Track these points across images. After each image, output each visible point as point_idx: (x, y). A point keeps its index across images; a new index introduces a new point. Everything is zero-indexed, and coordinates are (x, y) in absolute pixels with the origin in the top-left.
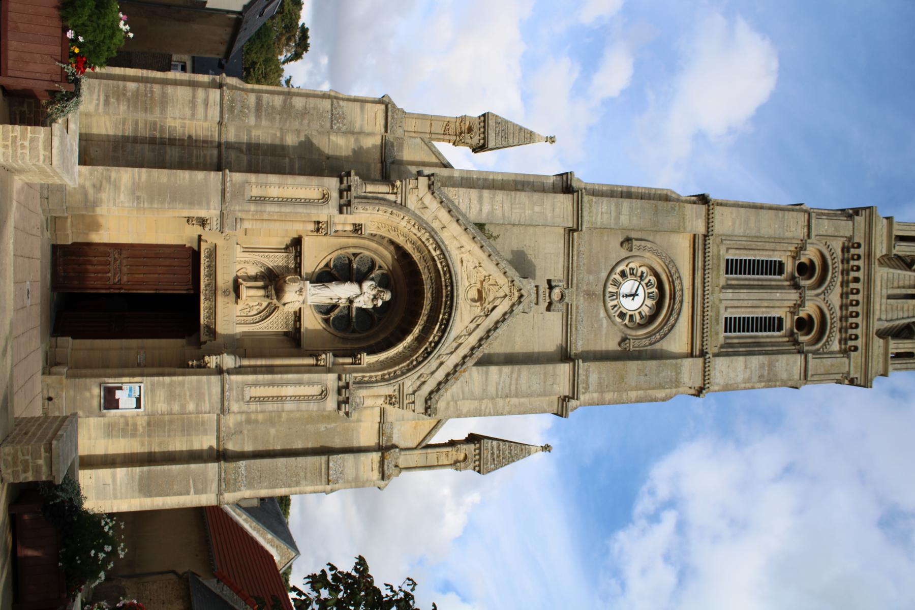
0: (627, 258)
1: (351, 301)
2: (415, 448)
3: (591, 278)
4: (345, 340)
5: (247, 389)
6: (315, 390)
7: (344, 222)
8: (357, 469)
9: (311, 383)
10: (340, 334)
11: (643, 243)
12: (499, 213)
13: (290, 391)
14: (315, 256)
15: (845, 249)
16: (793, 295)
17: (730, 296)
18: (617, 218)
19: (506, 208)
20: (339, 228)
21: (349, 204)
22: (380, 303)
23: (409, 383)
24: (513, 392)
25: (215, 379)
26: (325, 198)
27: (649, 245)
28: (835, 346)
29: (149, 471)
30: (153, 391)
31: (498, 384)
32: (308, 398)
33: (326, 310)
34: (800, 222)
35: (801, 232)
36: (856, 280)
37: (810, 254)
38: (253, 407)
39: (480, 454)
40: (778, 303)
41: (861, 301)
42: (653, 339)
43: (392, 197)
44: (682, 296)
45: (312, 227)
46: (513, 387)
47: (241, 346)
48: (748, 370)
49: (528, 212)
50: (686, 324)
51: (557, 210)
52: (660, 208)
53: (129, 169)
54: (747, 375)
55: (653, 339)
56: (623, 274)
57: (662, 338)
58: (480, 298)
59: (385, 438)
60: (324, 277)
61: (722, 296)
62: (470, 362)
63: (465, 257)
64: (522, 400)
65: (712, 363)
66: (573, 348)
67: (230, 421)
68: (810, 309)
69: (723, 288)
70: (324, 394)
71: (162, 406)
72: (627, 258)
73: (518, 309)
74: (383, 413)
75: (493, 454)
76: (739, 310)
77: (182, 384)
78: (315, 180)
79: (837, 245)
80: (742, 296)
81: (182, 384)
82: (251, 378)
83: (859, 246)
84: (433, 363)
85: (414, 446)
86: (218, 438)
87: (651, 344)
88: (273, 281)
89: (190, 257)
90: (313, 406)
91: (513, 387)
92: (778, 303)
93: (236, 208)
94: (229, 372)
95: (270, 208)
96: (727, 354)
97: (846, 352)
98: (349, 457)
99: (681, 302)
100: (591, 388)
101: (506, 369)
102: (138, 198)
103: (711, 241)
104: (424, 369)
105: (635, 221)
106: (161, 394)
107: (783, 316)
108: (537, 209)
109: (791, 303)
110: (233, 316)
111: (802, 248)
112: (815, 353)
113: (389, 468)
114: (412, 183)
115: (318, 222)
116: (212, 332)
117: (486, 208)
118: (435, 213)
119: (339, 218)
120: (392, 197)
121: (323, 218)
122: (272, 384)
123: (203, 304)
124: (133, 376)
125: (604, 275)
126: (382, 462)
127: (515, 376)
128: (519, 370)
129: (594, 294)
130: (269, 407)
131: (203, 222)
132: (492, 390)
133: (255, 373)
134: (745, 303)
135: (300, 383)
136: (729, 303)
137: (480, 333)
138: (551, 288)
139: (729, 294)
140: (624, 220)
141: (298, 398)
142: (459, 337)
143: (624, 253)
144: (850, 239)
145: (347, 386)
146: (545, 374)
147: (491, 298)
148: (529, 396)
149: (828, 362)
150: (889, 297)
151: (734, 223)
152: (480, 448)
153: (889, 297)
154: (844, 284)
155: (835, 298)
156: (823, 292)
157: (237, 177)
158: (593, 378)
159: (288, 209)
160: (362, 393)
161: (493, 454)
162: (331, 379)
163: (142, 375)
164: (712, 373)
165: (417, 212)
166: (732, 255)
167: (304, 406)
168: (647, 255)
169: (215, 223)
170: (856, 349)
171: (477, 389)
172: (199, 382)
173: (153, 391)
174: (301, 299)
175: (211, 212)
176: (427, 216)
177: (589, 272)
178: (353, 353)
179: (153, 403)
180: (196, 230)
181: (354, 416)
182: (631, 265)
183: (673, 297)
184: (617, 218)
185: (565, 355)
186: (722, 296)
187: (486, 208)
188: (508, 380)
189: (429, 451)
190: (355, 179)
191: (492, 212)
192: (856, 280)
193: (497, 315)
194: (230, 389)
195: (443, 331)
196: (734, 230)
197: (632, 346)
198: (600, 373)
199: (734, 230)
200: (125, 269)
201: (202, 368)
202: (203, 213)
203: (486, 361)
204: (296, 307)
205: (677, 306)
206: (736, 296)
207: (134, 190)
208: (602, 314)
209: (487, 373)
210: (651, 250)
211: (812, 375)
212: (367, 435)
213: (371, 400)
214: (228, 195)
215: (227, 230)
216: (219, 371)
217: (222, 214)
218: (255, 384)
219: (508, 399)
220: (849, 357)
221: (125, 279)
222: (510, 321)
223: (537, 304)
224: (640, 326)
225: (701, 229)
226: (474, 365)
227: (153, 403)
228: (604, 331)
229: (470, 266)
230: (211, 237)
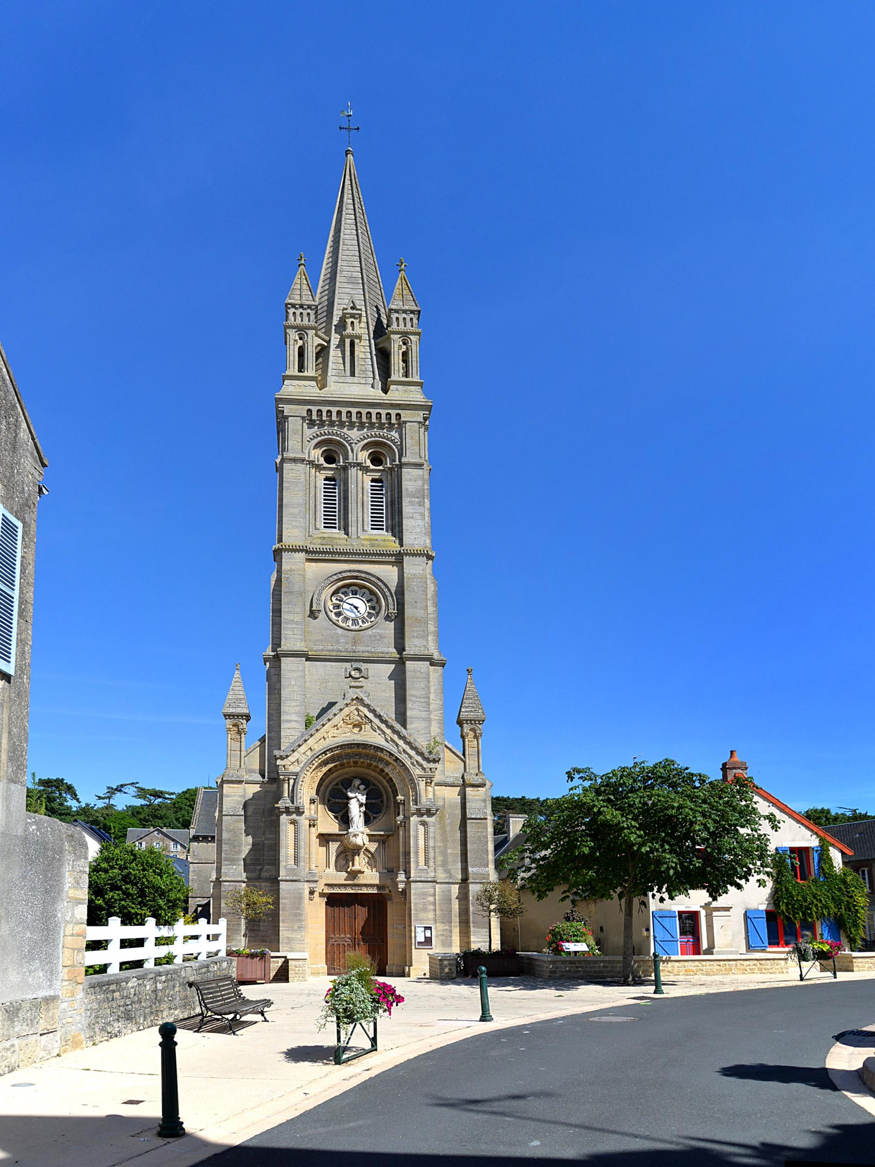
0: (326, 613)
1: (361, 805)
2: (465, 762)
3: (342, 640)
4: (388, 807)
5: (420, 867)
6: (421, 829)
7: (309, 810)
8: (477, 800)
9: (417, 831)
10: (384, 810)
11: (314, 601)
12: (297, 709)
13: (421, 843)
14: (329, 824)
15: (312, 424)
16: (353, 472)
17: (354, 529)
18: (297, 623)
19: (294, 704)
20: (313, 812)
21: (297, 808)
22: (362, 787)
23: (417, 772)
24: (426, 700)
25: (413, 885)
26: (294, 822)
27: (316, 596)
28: (395, 434)
29: (473, 923)
30: (420, 920)
31: (420, 710)
32: (426, 833)
33: (367, 822)
34: (292, 467)
35: (300, 467)
36: (339, 413)
37: (317, 455)
38: (431, 864)
39: (471, 721)
40: (361, 484)
41: (358, 410)
42: (388, 594)
43: (292, 782)
44: (354, 571)
45: (312, 829)
46: (423, 700)
47: (390, 872)
48: (415, 515)
49: (296, 688)
50: (369, 1060)
51: (293, 668)
52: (287, 590)
53: (281, 933)
54: (419, 517)
55: (388, 594)
56: (338, 614)
57: (387, 587)
58: (358, 725)
59: (456, 782)
60: (345, 820)
61: (354, 537)
62: (403, 732)
63: (331, 734)
64: (432, 691)
65: (409, 548)
66: (393, 655)
67: (441, 876)
68: (363, 457)
69: (347, 534)
70: (424, 824)
71: (431, 915)
72: (326, 613)
73: (367, 701)
74: (437, 785)
75: (471, 711)
76: (365, 519)
77: (416, 904)
78: (282, 828)
79: (309, 432)
80: (354, 518)
81: (416, 904)
82: (412, 865)
83: (309, 411)
84: (403, 757)
85: (463, 764)
86: (453, 883)
87: (392, 596)
88: (347, 853)
89: (333, 901)
90: (431, 829)
91: (423, 700)
92: (361, 484)
93: (304, 873)
94: (408, 877)
95: (302, 853)
96: (401, 532)
97: (401, 425)
98: (468, 805)
99: (359, 571)
100: (425, 643)
101: (409, 705)
102: (299, 927)
103: (311, 547)
104: (408, 763)
105: (298, 610)
106: (422, 915)
107: (370, 478)
108: (293, 683)
109: (360, 473)
110: (370, 877)
111: (311, 463)
112: (401, 456)
113: (478, 780)
114: (281, 770)
115: (310, 825)
116: (378, 887)
117: (294, 717)
118: (302, 755)
119: (307, 813)
120: (292, 782)
121: (307, 822)
122: (417, 853)
123: (365, 891)
124: (411, 931)
125: (340, 631)
126: (473, 786)
127: (414, 699)
128: (410, 696)
129: (354, 638)
130: (431, 855)
131: (312, 893)
132: (424, 715)
133: (409, 863)
134: (360, 515)
135: (416, 837)
136: (360, 530)
137: (383, 727)
138: (350, 676)
139: (352, 530)
140: (297, 618)
141: (426, 839)
142: (386, 740)
143: (322, 615)
144: (303, 418)
145: (419, 810)
146: (413, 678)
147: (359, 718)
148: (429, 687)
149: (409, 442)
150: (353, 374)
151: (297, 527)
152: (467, 721)
153: (353, 374)
154: (342, 424)
155: (354, 434)
156: (350, 444)
157: (282, 872)
158: (417, 642)
159: (302, 844)
160: (424, 799)
161: (471, 711)
162: (414, 819)
163: (410, 926)
164: (416, 548)
165: (301, 765)
166: (321, 524)
167: (431, 835)
168: (323, 597)
169: (313, 885)
170: (398, 415)
171: (423, 724)
172: (414, 894)
173: (420, 920)
174: (360, 835)
175: (306, 887)
176: (304, 759)
177: (338, 642)
178: (397, 805)
179: (428, 920)
180: (316, 894)
181: (440, 803)
182: (331, 608)
183: (356, 578)
184: (297, 623)
185: (400, 663)
186: (354, 537)
187: (294, 717)
188: (417, 704)
189: (467, 753)
190: (281, 804)
191: (297, 713)
192: (339, 413)
193: (370, 716)
194: (420, 877)
195: (382, 750)
196: (301, 527)
197: (393, 610)
198: (413, 637)
199: (301, 527)
200: (342, 936)
201: (405, 893)
202: (307, 892)
203: (402, 717)
204: (366, 839)
205: (363, 575)
206: (354, 524)
207: (292, 929)
208: (369, 632)
209: (412, 718)
210: (320, 594)
211: (420, 457)
212: (452, 795)
213: (427, 794)
214: (295, 878)
215: (317, 879)
216: (408, 882)
217: (307, 881)
218: (417, 863)
219: (431, 701)
220: (405, 422)
221: (348, 936)
222: (373, 705)
223: (362, 687)
224: (378, 601)
225: (302, 555)
226: (405, 728)
227: (428, 920)
228: (382, 631)
229: (336, 733)
230: (320, 887)
